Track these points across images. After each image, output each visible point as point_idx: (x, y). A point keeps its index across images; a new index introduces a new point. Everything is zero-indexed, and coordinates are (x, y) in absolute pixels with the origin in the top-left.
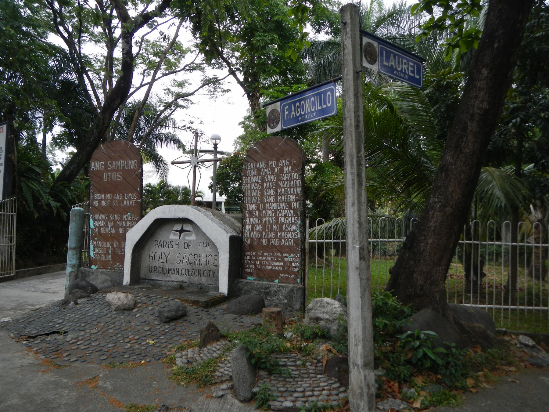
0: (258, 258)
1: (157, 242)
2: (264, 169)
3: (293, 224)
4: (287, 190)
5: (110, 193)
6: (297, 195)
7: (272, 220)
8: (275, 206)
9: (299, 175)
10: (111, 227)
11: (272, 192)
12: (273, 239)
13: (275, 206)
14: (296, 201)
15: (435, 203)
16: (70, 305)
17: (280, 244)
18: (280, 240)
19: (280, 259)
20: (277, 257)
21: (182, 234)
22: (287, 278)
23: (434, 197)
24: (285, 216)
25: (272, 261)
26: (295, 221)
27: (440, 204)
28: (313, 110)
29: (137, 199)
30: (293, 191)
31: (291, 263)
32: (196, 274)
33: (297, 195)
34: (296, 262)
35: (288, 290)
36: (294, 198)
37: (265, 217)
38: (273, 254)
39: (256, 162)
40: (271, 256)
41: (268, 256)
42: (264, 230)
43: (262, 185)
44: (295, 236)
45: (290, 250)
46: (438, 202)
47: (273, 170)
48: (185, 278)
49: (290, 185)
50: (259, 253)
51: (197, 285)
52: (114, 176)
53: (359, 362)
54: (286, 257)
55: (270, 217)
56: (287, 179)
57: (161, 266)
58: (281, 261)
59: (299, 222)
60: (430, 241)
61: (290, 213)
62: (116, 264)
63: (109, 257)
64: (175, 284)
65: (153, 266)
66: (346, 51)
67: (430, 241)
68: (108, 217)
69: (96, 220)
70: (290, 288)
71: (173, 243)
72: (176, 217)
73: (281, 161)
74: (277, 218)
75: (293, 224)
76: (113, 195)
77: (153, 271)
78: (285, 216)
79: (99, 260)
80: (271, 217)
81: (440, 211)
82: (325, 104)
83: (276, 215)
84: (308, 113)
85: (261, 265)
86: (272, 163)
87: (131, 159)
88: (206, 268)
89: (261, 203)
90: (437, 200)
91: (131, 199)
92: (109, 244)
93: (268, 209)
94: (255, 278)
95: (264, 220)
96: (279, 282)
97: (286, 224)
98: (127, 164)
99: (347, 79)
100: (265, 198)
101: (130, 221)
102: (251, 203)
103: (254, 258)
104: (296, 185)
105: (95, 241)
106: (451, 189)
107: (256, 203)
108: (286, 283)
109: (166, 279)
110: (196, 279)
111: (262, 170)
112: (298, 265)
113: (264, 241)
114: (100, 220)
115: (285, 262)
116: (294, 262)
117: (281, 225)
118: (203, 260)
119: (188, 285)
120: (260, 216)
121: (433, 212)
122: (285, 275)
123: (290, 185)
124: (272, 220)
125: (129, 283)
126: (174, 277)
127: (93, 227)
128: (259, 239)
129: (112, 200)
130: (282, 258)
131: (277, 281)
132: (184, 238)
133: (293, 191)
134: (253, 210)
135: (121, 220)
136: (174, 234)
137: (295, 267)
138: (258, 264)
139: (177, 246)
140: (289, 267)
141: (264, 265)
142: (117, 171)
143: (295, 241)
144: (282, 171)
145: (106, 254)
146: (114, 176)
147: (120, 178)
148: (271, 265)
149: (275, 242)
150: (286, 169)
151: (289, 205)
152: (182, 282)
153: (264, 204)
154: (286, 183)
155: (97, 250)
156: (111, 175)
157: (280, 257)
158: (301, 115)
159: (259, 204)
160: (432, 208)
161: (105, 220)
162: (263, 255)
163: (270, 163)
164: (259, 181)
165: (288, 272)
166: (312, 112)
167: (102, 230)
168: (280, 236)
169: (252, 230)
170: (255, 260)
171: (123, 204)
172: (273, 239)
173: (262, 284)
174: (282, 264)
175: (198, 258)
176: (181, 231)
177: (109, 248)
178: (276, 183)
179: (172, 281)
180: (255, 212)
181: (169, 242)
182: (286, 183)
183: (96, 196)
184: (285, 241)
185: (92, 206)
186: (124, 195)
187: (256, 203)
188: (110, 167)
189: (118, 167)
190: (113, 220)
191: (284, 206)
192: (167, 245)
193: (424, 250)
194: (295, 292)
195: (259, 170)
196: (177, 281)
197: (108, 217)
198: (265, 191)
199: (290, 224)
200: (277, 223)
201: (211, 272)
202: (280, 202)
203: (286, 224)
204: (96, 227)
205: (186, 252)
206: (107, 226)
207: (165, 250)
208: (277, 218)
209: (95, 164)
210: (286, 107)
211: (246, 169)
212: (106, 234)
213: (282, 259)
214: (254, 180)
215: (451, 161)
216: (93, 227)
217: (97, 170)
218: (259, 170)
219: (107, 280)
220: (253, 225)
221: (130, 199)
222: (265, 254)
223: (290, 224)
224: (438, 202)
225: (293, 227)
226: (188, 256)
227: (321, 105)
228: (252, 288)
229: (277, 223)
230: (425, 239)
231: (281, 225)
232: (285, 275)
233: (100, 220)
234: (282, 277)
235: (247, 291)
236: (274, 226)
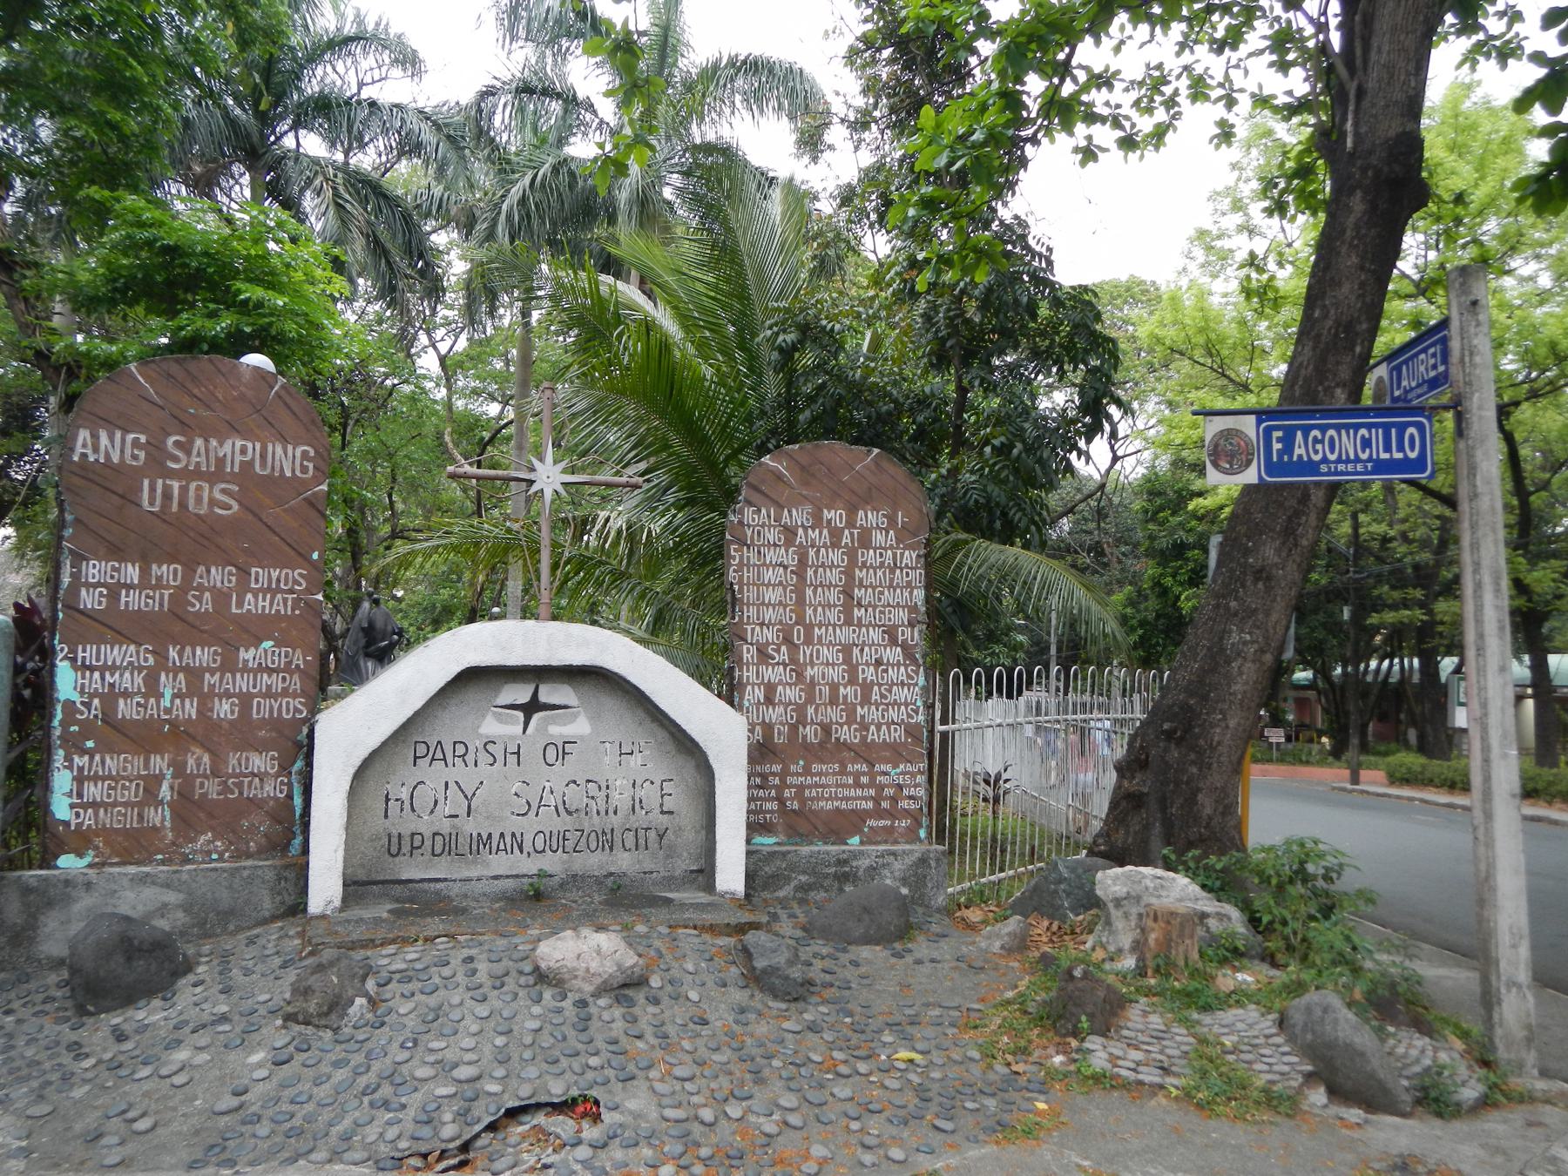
0: (789, 780)
1: (422, 750)
2: (805, 529)
3: (903, 684)
4: (882, 593)
5: (172, 559)
6: (913, 609)
7: (835, 674)
8: (845, 635)
9: (918, 556)
10: (175, 696)
11: (833, 596)
12: (841, 725)
13: (845, 635)
14: (911, 624)
15: (1245, 643)
16: (351, 1011)
17: (864, 738)
18: (864, 727)
19: (864, 780)
20: (857, 775)
21: (536, 717)
22: (889, 830)
23: (1242, 631)
24: (878, 663)
25: (837, 786)
26: (909, 677)
27: (1256, 646)
28: (1364, 456)
29: (308, 591)
30: (902, 596)
31: (900, 787)
32: (593, 845)
33: (913, 609)
34: (916, 786)
35: (909, 860)
36: (903, 616)
37: (812, 664)
38: (843, 766)
39: (780, 507)
40: (835, 774)
41: (827, 774)
42: (810, 699)
43: (800, 572)
44: (909, 716)
45: (896, 753)
46: (1252, 642)
47: (836, 534)
48: (552, 863)
49: (892, 580)
50: (793, 768)
51: (599, 881)
52: (199, 499)
53: (1523, 976)
54: (885, 774)
55: (828, 664)
56: (882, 563)
57: (445, 831)
58: (868, 786)
59: (921, 681)
60: (1232, 723)
61: (893, 654)
62: (194, 840)
63: (159, 817)
64: (510, 884)
65: (406, 832)
66: (1478, 359)
67: (1232, 723)
68: (161, 655)
69: (92, 669)
70: (917, 855)
71: (497, 750)
72: (554, 663)
73: (861, 513)
74: (852, 669)
75: (903, 684)
76: (190, 570)
77: (406, 849)
78: (878, 663)
79: (104, 832)
80: (833, 664)
81: (1254, 661)
82: (1401, 448)
83: (847, 660)
84: (1348, 461)
85: (803, 801)
86: (835, 515)
87: (284, 440)
88: (634, 822)
89: (797, 623)
90: (1248, 637)
91: (278, 590)
92: (159, 763)
93: (820, 642)
94: (782, 838)
95: (809, 672)
96: (862, 843)
97: (880, 685)
98: (263, 456)
99: (1481, 418)
100: (809, 612)
101: (270, 671)
102: (762, 624)
103: (777, 781)
104: (909, 583)
105: (83, 752)
106: (1274, 617)
107: (781, 622)
108: (886, 842)
109: (466, 874)
110: (593, 862)
111: (800, 531)
112: (921, 792)
113: (810, 733)
114: (113, 668)
115: (881, 787)
116: (909, 786)
117: (867, 688)
118: (621, 798)
119: (561, 885)
120: (794, 660)
121: (1240, 661)
122: (882, 823)
123: (892, 580)
124: (835, 674)
125: (337, 903)
126: (500, 864)
127: (76, 697)
128: (794, 728)
129: (183, 589)
130: (872, 775)
131: (855, 840)
132: (542, 730)
133: (902, 596)
134: (768, 644)
135: (229, 665)
136: (499, 718)
137: (911, 798)
138: (792, 799)
139: (512, 759)
140: (894, 800)
141: (812, 799)
142: (214, 477)
143: (911, 731)
144: (865, 541)
145: (141, 805)
146: (199, 499)
147: (228, 507)
148: (837, 798)
149: (846, 734)
150: (878, 538)
151: (891, 635)
152: (542, 874)
153: (809, 628)
154: (880, 573)
155: (93, 791)
156: (184, 490)
157: (864, 774)
158: (1325, 460)
159: (792, 627)
160: (1239, 654)
161: (140, 669)
162: (807, 771)
163: (827, 514)
164: (791, 560)
165: (891, 814)
166: (1357, 460)
167: (124, 709)
168: (863, 717)
169: (769, 700)
170: (780, 789)
171: (240, 604)
172: (841, 725)
173: (828, 853)
174: (872, 792)
175: (603, 793)
176: (531, 708)
177: (159, 778)
178: (848, 573)
179: (496, 877)
180: (778, 651)
181: (480, 745)
182: (880, 573)
183: (94, 570)
184: (879, 729)
185: (72, 607)
186: (244, 572)
187: (781, 622)
188: (176, 459)
189: (221, 462)
190: (187, 670)
191: (875, 635)
192: (470, 758)
193: (1219, 743)
194: (933, 864)
195: (790, 532)
196: (517, 876)
197: (161, 655)
198: (809, 592)
199: (893, 684)
200: (852, 681)
201: (652, 835)
202: (860, 625)
203: (880, 685)
204: (92, 696)
205: (556, 778)
206: (152, 689)
207: (458, 772)
208: (852, 669)
209: (95, 437)
210: (1277, 434)
211: (741, 523)
212: (147, 724)
213: (873, 779)
214: (771, 556)
215: (1276, 560)
216: (76, 697)
217: (108, 463)
218: (790, 532)
219: (165, 905)
220: (770, 689)
221: (272, 591)
222: (815, 767)
223: (893, 684)
224: (1252, 642)
225: (902, 694)
226: (559, 788)
227: (1388, 449)
228: (792, 868)
229: (852, 681)
230: (1224, 719)
231: (867, 688)
232: (882, 823)
233: (113, 668)
234: (871, 828)
235: (772, 876)
236: (842, 689)
